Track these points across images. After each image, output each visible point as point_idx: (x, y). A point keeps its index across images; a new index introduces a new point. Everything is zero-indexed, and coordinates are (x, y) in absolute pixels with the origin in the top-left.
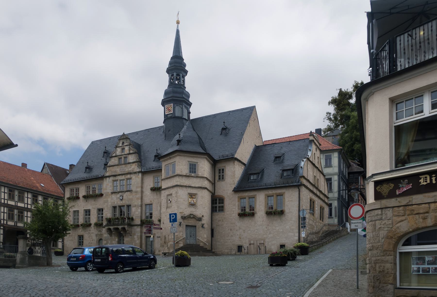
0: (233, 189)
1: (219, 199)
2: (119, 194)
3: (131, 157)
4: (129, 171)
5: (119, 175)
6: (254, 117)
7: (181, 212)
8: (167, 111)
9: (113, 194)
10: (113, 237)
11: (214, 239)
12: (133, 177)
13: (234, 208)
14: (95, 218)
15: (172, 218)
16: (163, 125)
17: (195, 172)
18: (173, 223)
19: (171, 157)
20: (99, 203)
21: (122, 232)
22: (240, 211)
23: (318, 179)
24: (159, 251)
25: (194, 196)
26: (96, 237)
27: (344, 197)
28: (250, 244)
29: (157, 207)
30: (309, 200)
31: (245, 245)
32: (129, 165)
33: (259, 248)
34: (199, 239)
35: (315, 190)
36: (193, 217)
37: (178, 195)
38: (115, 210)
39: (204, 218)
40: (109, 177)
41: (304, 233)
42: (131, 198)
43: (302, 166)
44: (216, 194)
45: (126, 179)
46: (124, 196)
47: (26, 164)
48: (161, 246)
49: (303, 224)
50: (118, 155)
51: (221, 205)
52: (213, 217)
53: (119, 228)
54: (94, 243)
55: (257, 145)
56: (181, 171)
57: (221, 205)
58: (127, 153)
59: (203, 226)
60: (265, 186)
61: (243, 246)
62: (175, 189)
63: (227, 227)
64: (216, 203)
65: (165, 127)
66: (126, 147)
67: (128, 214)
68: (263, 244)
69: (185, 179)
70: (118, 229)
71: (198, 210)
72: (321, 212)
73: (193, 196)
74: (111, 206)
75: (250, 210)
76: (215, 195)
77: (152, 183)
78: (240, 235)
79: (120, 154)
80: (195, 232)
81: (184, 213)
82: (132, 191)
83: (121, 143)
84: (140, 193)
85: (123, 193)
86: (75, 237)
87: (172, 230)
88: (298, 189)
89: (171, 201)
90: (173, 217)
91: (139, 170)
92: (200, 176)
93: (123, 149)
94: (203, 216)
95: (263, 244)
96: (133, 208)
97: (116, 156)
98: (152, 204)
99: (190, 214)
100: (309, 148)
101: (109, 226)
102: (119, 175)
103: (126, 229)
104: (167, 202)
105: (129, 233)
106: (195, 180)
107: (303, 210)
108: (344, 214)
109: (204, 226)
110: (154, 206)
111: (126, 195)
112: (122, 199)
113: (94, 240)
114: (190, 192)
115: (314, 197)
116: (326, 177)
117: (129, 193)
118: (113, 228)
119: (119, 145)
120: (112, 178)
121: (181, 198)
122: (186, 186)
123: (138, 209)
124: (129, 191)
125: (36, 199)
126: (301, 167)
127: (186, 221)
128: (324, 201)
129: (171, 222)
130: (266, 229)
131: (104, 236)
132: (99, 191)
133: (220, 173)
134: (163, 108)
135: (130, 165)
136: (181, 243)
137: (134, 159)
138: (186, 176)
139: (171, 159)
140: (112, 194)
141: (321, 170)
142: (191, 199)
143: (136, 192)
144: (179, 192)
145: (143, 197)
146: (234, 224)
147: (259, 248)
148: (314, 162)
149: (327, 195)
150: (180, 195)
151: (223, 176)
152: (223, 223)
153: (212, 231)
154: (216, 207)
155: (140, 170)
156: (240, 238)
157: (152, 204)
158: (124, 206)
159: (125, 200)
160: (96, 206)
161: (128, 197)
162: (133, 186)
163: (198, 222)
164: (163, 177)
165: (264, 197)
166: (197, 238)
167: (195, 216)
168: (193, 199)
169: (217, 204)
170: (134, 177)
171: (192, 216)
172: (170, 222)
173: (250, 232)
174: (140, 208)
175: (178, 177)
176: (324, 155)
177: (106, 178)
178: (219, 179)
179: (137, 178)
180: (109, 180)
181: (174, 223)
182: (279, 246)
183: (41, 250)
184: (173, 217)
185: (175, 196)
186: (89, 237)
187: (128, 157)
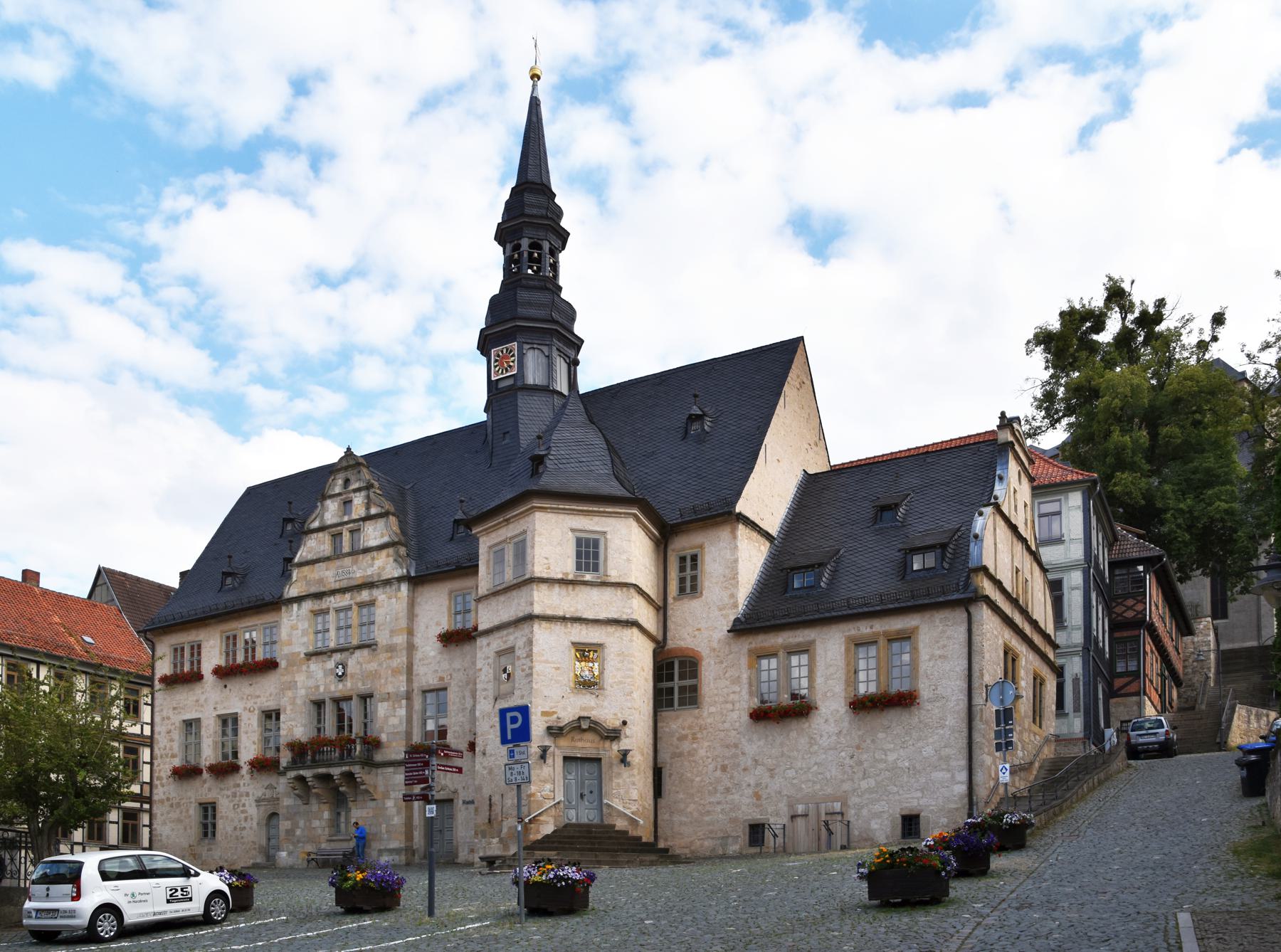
2: (333, 659)
7: (547, 709)
10: (314, 806)
11: (662, 802)
13: (734, 693)
20: (265, 691)
25: (591, 653)
26: (256, 809)
29: (464, 698)
42: (372, 669)
46: (349, 664)
50: (329, 522)
54: (251, 828)
57: (688, 682)
63: (710, 760)
66: (358, 494)
67: (365, 725)
69: (560, 595)
71: (606, 704)
73: (589, 651)
78: (758, 785)
81: (555, 716)
92: (613, 580)
111: (356, 662)
112: (343, 674)
117: (366, 652)
119: (333, 489)
120: (308, 605)
121: (547, 662)
123: (396, 706)
130: (852, 762)
133: (682, 569)
136: (547, 823)
139: (511, 526)
142: (583, 663)
146: (736, 746)
151: (694, 578)
152: (695, 746)
159: (352, 677)
160: (256, 703)
163: (607, 744)
167: (596, 723)
168: (591, 664)
170: (383, 596)
171: (585, 725)
173: (791, 773)
178: (682, 590)
179: (394, 600)
180: (300, 612)
186: (234, 809)
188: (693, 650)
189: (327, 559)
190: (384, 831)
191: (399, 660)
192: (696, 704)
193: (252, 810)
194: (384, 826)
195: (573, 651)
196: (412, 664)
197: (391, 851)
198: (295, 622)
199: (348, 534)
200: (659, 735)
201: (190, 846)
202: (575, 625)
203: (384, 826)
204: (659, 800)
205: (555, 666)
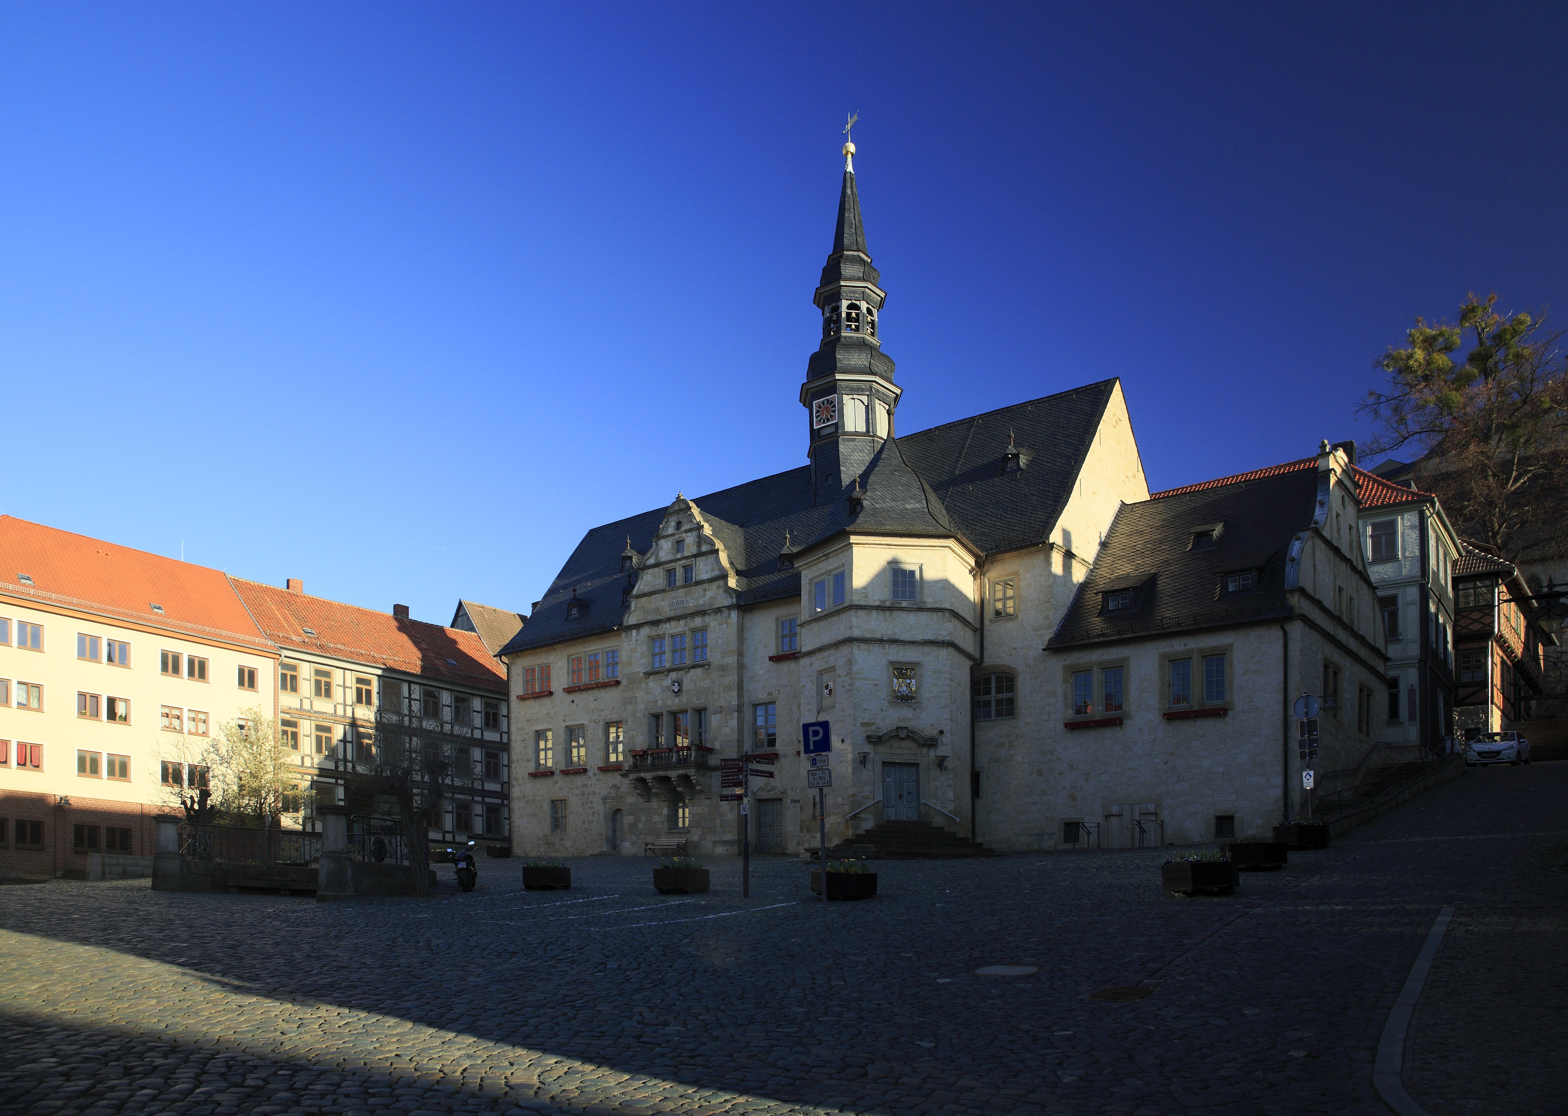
0: (1046, 643)
1: (997, 678)
2: (669, 677)
3: (706, 565)
4: (700, 605)
5: (669, 620)
6: (1114, 415)
7: (866, 721)
8: (819, 419)
9: (652, 677)
12: (712, 624)
13: (1049, 705)
14: (599, 750)
15: (812, 739)
16: (807, 462)
17: (912, 595)
18: (816, 755)
19: (829, 553)
21: (679, 789)
22: (1070, 714)
23: (1351, 599)
24: (799, 844)
25: (909, 671)
27: (1442, 656)
28: (1106, 816)
30: (1321, 668)
31: (1091, 818)
32: (700, 588)
33: (1141, 827)
34: (929, 806)
35: (1342, 635)
36: (907, 737)
37: (855, 669)
38: (658, 725)
39: (944, 738)
40: (638, 626)
41: (1311, 776)
43: (1293, 555)
44: (987, 662)
45: (690, 630)
46: (685, 681)
47: (407, 608)
48: (802, 829)
49: (1307, 744)
50: (663, 560)
51: (1004, 696)
52: (976, 734)
53: (670, 778)
55: (1128, 501)
56: (864, 595)
57: (1004, 696)
58: (690, 554)
59: (941, 763)
60: (1158, 628)
61: (1081, 825)
62: (845, 650)
64: (988, 692)
65: (813, 468)
66: (689, 534)
67: (700, 734)
68: (1154, 816)
70: (667, 779)
72: (1360, 706)
73: (906, 669)
74: (646, 713)
75: (1108, 707)
76: (984, 665)
77: (774, 637)
79: (670, 557)
80: (914, 784)
81: (875, 726)
82: (709, 664)
83: (673, 524)
84: (735, 671)
85: (681, 673)
86: (542, 807)
87: (814, 778)
88: (1280, 633)
89: (830, 691)
90: (816, 733)
91: (730, 600)
92: (929, 606)
93: (680, 543)
94: (941, 732)
95: (1154, 816)
96: (713, 716)
97: (656, 565)
98: (774, 703)
99: (898, 728)
100: (1319, 498)
101: (640, 771)
102: (669, 620)
103: (692, 778)
104: (818, 694)
105: (702, 791)
106: (911, 618)
107: (1307, 696)
108: (1442, 710)
109: (946, 763)
110: (780, 708)
112: (679, 690)
113: (598, 814)
114: (895, 659)
115: (1337, 657)
116: (1380, 593)
118: (654, 778)
119: (667, 530)
120: (645, 631)
122: (881, 641)
123: (728, 717)
124: (702, 666)
125: (493, 713)
126: (1293, 560)
127: (882, 749)
128: (1372, 670)
129: (812, 752)
131: (628, 801)
132: (607, 670)
134: (806, 411)
135: (701, 589)
137: (713, 570)
138: (880, 608)
139: (830, 560)
140: (647, 678)
141: (1360, 568)
142: (901, 680)
143: (723, 668)
144: (860, 662)
145: (745, 684)
147: (1141, 827)
148: (1335, 543)
149: (1383, 651)
150: (862, 669)
152: (1011, 752)
153: (975, 777)
154: (988, 704)
155: (734, 600)
156: (1073, 797)
157: (774, 703)
158: (685, 711)
161: (698, 683)
162: (711, 652)
164: (805, 616)
165: (1157, 664)
166: (923, 801)
167: (913, 732)
168: (908, 681)
169: (989, 693)
170: (715, 622)
171: (903, 734)
172: (807, 751)
174: (735, 714)
175: (852, 612)
176: (1369, 522)
177: (629, 632)
179: (724, 626)
181: (821, 755)
182: (1213, 821)
183: (397, 846)
184: (816, 733)
185: (845, 674)
186: (583, 805)
187: (694, 565)
188: (1009, 667)
189: (663, 591)
190: (718, 825)
191: (730, 678)
192: (1013, 715)
193: (599, 806)
194: (718, 821)
195: (891, 669)
196: (743, 681)
197: (724, 843)
198: (634, 646)
199: (681, 569)
200: (976, 742)
201: (544, 836)
202: (892, 646)
203: (718, 821)
204: (976, 800)
205: (874, 682)
